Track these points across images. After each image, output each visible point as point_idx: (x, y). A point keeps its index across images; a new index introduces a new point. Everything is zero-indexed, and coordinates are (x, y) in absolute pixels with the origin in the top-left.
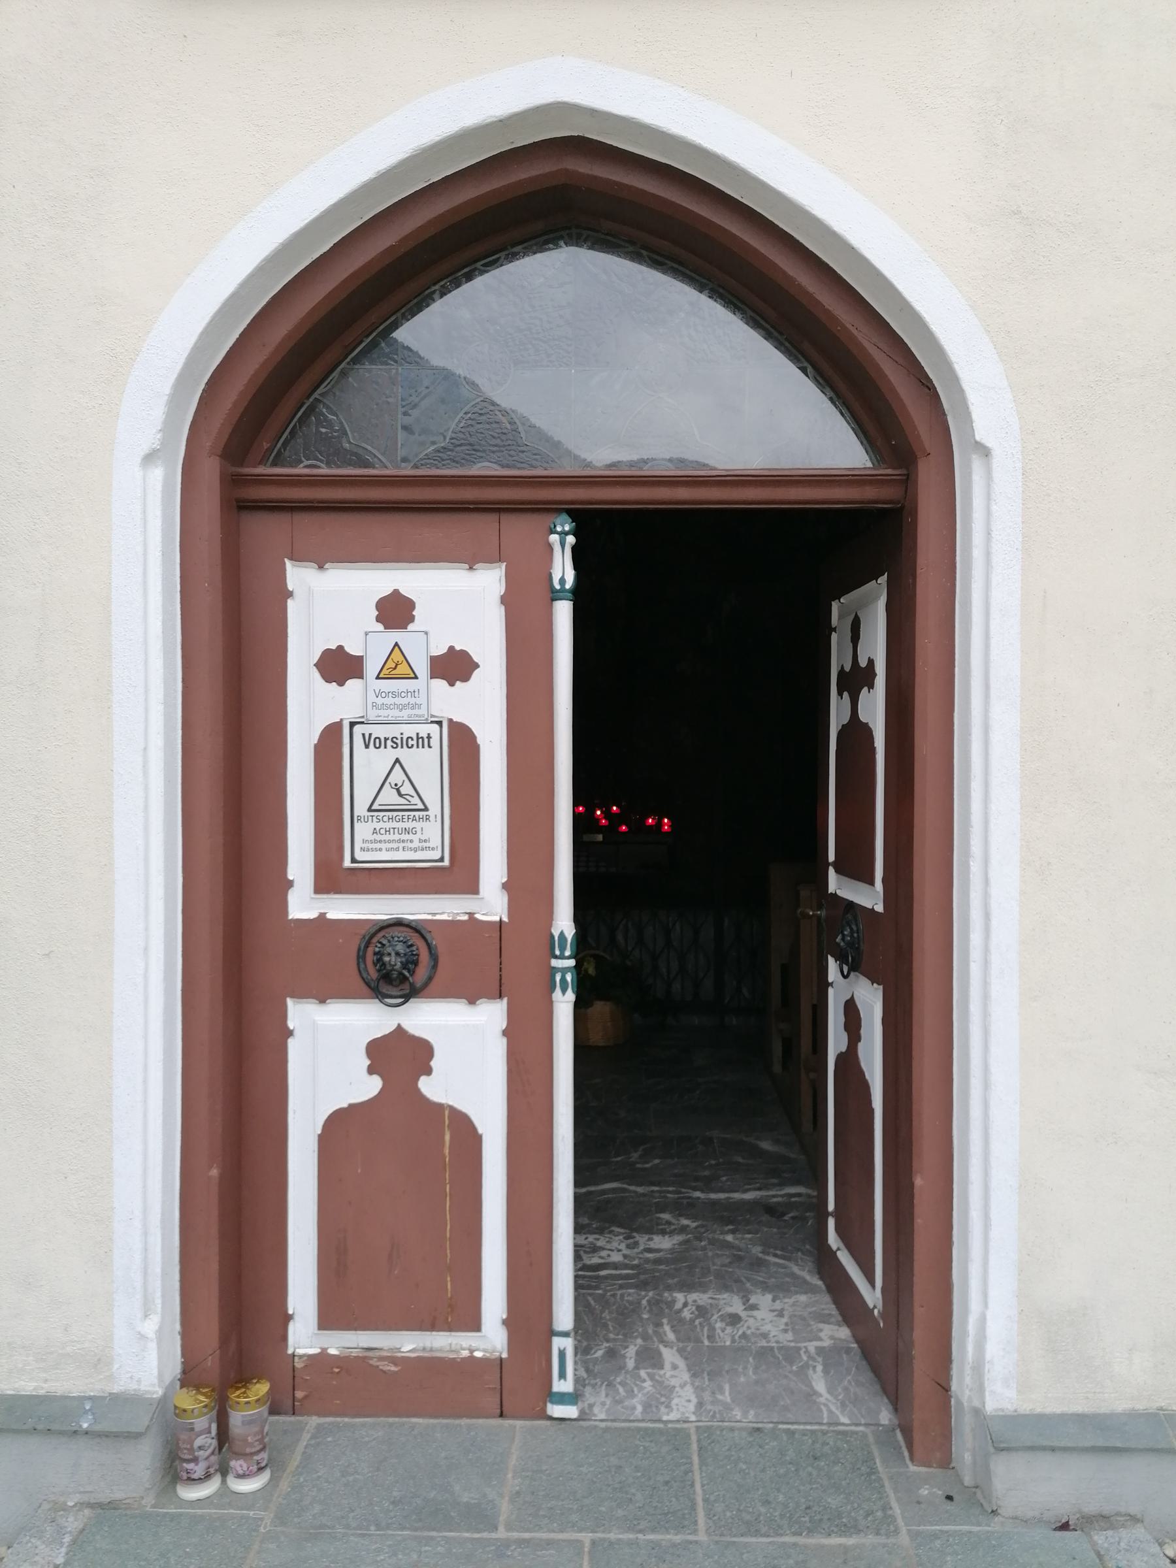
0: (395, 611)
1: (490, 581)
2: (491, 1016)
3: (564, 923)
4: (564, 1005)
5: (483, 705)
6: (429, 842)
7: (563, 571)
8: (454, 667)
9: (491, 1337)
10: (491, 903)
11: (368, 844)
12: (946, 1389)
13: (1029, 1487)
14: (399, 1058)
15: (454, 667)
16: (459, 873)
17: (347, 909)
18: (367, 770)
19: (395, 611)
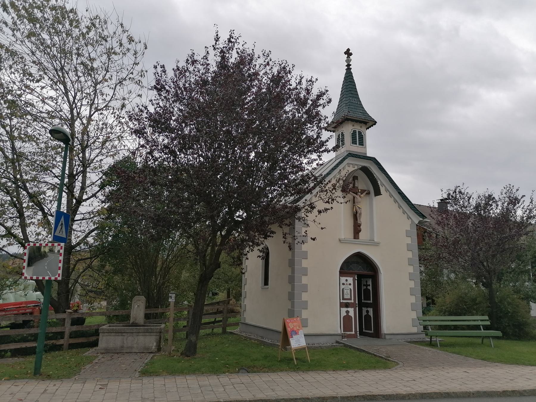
0: (347, 280)
1: (352, 278)
2: (353, 309)
3: (357, 302)
4: (357, 308)
5: (351, 287)
6: (349, 297)
7: (356, 278)
8: (350, 284)
9: (353, 333)
10: (352, 301)
11: (345, 297)
12: (412, 204)
13: (387, 337)
14: (347, 312)
15: (350, 284)
16: (350, 299)
17: (344, 301)
18: (345, 291)
19: (347, 280)
